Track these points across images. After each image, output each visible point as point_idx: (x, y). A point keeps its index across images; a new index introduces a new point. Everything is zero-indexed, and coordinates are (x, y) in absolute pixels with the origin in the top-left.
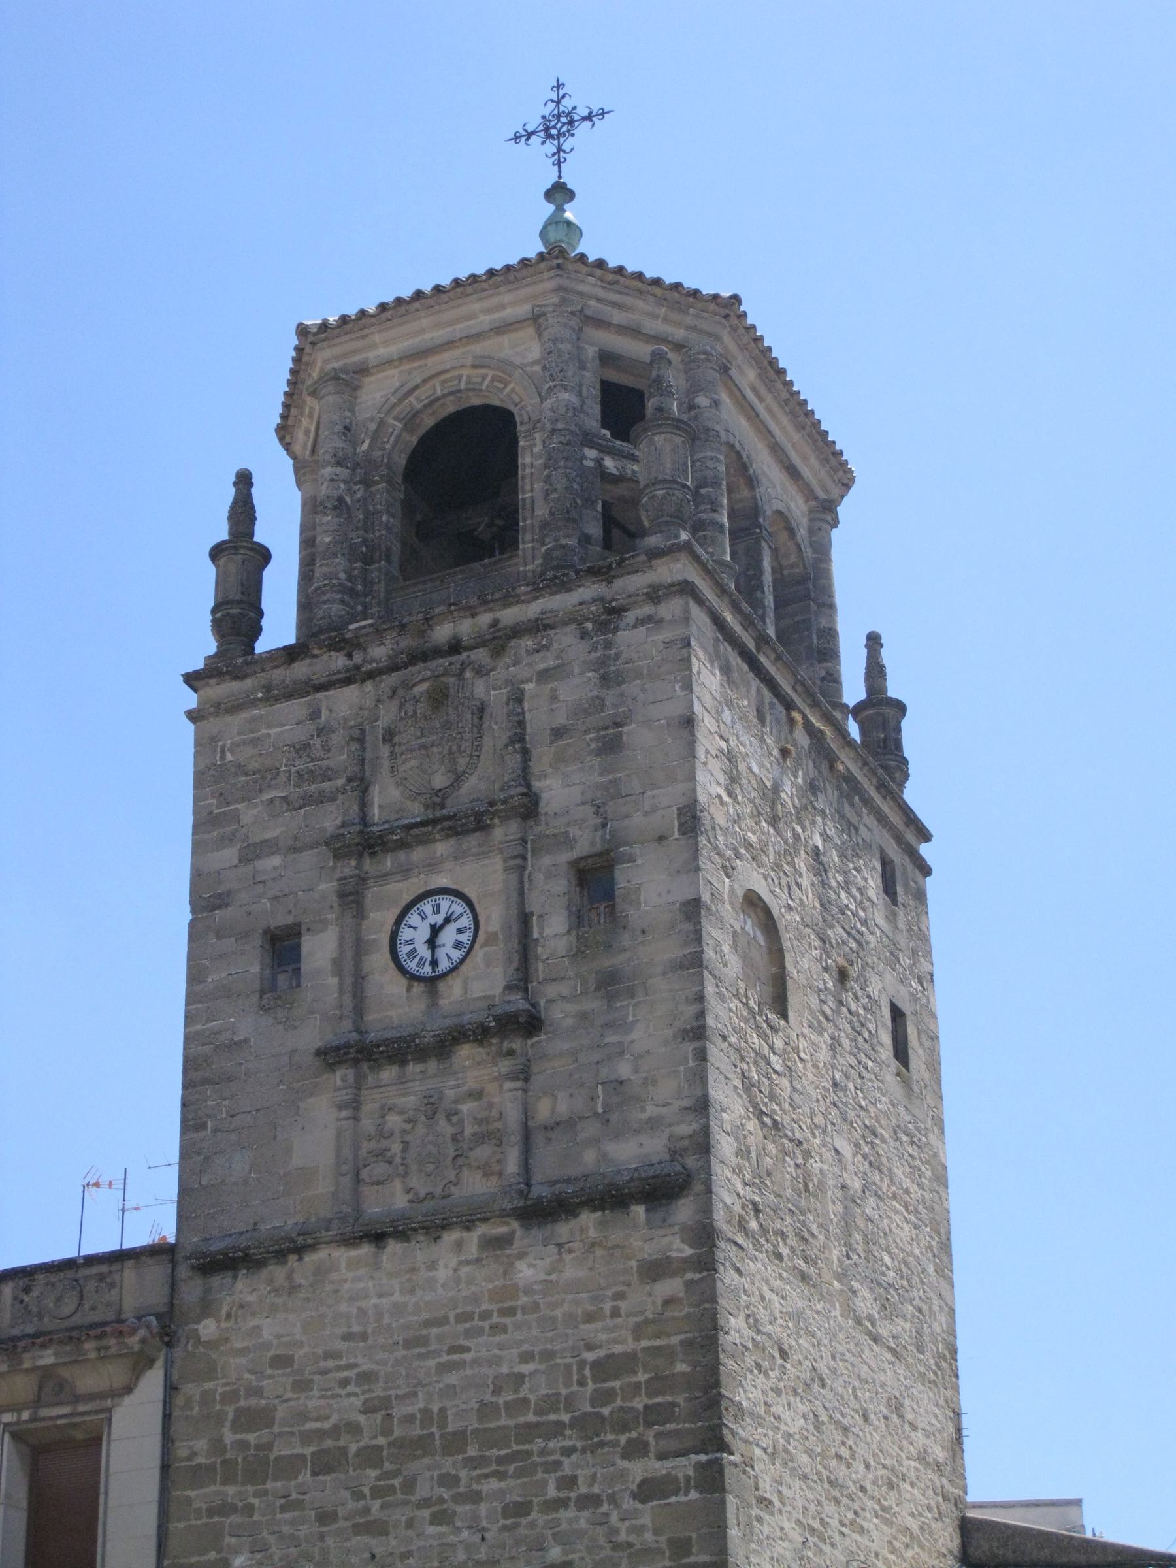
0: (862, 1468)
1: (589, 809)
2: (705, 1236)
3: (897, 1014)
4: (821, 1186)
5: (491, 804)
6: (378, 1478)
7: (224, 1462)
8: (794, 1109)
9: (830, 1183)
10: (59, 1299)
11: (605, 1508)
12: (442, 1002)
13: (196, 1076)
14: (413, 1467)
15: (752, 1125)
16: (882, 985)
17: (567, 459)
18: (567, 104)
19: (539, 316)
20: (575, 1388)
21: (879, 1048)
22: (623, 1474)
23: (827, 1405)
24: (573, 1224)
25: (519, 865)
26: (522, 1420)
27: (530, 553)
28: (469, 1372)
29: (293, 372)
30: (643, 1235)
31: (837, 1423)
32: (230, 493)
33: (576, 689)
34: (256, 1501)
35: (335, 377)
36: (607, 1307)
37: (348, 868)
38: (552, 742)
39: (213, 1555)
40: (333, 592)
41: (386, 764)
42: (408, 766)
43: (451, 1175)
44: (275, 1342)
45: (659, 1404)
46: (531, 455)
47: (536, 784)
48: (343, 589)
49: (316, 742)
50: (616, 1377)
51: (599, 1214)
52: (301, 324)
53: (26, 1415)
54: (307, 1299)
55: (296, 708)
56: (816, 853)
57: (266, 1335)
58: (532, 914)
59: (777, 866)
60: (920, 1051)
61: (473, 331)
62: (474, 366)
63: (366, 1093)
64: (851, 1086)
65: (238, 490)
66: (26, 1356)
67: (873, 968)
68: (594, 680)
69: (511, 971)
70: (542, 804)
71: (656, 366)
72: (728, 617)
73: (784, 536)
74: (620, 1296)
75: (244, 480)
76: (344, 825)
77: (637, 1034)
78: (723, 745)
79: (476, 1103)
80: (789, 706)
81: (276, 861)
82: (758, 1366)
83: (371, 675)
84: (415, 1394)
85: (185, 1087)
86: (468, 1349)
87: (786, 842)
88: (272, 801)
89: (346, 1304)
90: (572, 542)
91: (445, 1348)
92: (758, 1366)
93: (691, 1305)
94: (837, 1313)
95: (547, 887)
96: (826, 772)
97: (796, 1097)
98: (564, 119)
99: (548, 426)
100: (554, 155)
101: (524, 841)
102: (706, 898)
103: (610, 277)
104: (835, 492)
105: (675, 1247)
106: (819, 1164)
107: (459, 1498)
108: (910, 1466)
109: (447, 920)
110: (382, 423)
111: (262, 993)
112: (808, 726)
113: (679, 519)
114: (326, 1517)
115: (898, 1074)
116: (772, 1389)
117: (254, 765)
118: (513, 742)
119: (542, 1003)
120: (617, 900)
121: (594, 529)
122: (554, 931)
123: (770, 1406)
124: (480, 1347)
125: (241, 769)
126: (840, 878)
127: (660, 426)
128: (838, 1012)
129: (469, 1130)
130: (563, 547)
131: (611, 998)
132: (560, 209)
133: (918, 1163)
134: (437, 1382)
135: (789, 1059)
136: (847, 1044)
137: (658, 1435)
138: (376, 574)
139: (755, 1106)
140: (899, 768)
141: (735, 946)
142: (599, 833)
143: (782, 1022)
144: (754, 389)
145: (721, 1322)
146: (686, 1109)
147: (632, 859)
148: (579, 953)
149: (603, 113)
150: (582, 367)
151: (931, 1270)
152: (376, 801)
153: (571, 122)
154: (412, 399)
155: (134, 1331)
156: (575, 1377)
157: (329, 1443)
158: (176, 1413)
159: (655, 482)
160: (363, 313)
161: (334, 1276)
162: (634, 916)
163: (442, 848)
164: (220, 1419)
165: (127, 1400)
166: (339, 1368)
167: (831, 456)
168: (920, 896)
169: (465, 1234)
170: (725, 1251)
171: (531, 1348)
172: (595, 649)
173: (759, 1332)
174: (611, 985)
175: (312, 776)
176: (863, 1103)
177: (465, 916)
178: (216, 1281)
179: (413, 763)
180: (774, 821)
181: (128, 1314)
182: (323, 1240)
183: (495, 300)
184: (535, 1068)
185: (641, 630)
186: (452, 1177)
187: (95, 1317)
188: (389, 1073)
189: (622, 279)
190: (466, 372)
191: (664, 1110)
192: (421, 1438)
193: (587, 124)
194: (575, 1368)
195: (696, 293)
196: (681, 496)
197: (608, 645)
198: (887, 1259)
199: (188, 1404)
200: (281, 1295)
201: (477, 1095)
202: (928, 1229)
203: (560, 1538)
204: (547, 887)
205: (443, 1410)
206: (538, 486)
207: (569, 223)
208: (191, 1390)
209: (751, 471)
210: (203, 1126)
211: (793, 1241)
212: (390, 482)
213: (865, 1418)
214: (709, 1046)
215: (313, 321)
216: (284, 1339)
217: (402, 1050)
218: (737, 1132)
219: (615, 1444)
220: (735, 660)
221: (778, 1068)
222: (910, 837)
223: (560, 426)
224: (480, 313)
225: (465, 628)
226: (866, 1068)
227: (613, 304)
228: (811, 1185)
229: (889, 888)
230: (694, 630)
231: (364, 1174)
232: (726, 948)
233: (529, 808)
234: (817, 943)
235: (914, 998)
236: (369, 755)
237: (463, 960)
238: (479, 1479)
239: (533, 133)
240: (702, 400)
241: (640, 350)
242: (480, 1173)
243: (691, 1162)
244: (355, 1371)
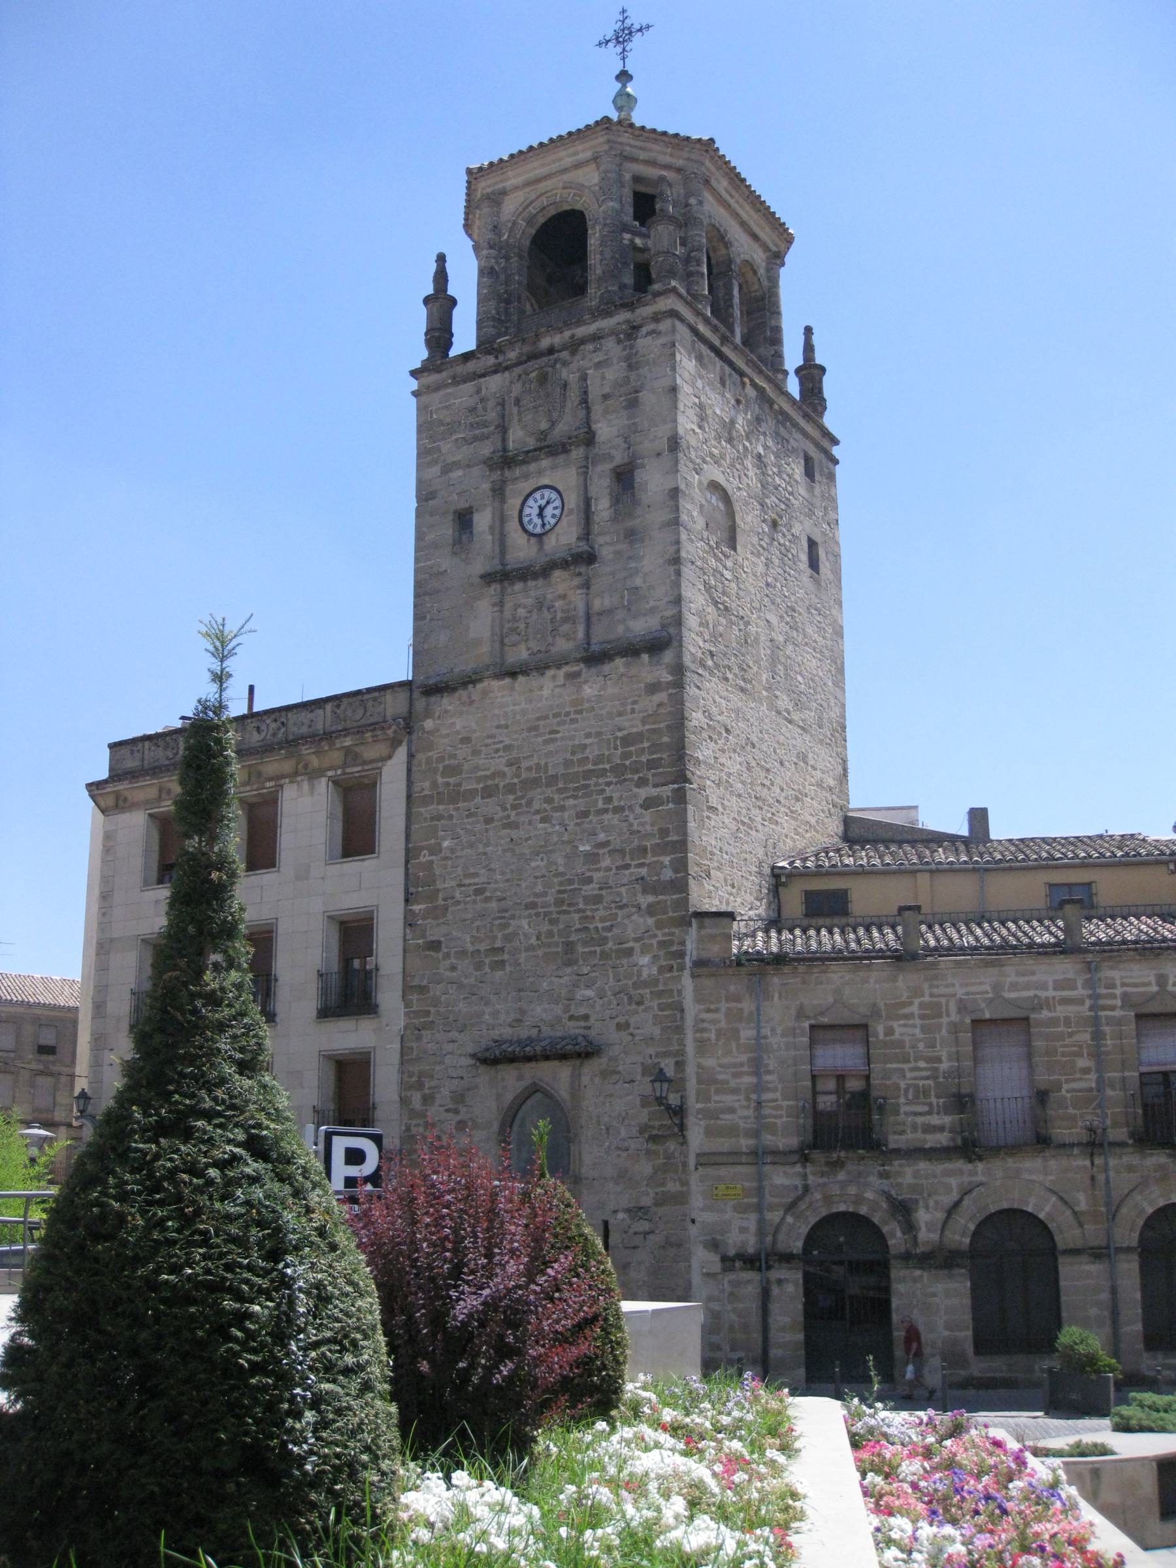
0: (778, 790)
1: (620, 440)
2: (679, 670)
3: (812, 544)
4: (757, 640)
5: (570, 438)
6: (515, 800)
7: (438, 793)
9: (763, 638)
10: (354, 711)
11: (627, 813)
12: (545, 547)
14: (531, 794)
15: (711, 609)
16: (801, 528)
18: (628, 22)
22: (635, 796)
24: (612, 665)
25: (585, 473)
26: (586, 768)
27: (594, 293)
29: (468, 195)
30: (649, 670)
31: (762, 767)
32: (433, 267)
33: (613, 373)
34: (454, 813)
35: (487, 197)
36: (629, 708)
37: (496, 475)
39: (433, 841)
41: (516, 418)
46: (593, 241)
47: (594, 426)
48: (494, 319)
49: (480, 406)
50: (633, 745)
53: (339, 772)
55: (469, 387)
56: (759, 456)
59: (732, 465)
64: (779, 585)
66: (337, 741)
72: (702, 328)
73: (750, 275)
74: (635, 702)
75: (441, 259)
76: (494, 452)
77: (645, 562)
78: (697, 400)
80: (742, 374)
81: (460, 473)
82: (710, 738)
83: (507, 368)
84: (532, 756)
85: (415, 597)
86: (558, 732)
87: (738, 451)
88: (457, 440)
90: (615, 288)
92: (710, 738)
94: (764, 708)
96: (767, 410)
97: (741, 593)
101: (587, 458)
102: (683, 487)
103: (637, 133)
104: (783, 246)
107: (555, 809)
108: (810, 789)
109: (548, 503)
110: (514, 223)
112: (754, 385)
113: (672, 274)
114: (489, 820)
117: (448, 420)
118: (581, 403)
119: (596, 546)
121: (628, 279)
122: (603, 507)
125: (441, 422)
126: (775, 470)
128: (771, 544)
131: (632, 543)
132: (624, 86)
133: (823, 625)
136: (776, 562)
137: (654, 775)
139: (713, 599)
140: (820, 404)
141: (701, 512)
144: (727, 192)
145: (687, 715)
147: (643, 466)
148: (614, 520)
149: (648, 27)
150: (623, 186)
151: (830, 684)
152: (511, 438)
153: (630, 33)
155: (389, 728)
157: (490, 782)
158: (414, 769)
159: (658, 253)
160: (501, 160)
161: (492, 695)
163: (545, 463)
164: (435, 771)
165: (389, 763)
166: (494, 743)
168: (831, 477)
170: (689, 677)
172: (625, 349)
173: (711, 720)
174: (632, 536)
175: (479, 425)
178: (433, 699)
179: (529, 417)
180: (730, 440)
181: (389, 718)
183: (572, 150)
184: (593, 581)
185: (649, 338)
187: (372, 720)
188: (518, 586)
190: (559, 191)
192: (535, 779)
193: (639, 34)
195: (688, 138)
197: (632, 347)
198: (800, 678)
199: (420, 765)
201: (563, 597)
203: (606, 829)
205: (546, 764)
206: (598, 257)
207: (629, 95)
208: (421, 757)
210: (425, 617)
211: (736, 670)
212: (521, 257)
213: (782, 764)
215: (475, 165)
217: (525, 574)
218: (700, 614)
219: (631, 780)
220: (705, 350)
221: (729, 577)
222: (825, 443)
223: (608, 221)
224: (566, 157)
225: (557, 339)
227: (641, 148)
229: (809, 473)
230: (678, 337)
231: (506, 641)
232: (695, 514)
233: (589, 439)
234: (759, 507)
235: (824, 534)
236: (507, 413)
238: (564, 799)
240: (693, 201)
241: (652, 172)
243: (672, 630)
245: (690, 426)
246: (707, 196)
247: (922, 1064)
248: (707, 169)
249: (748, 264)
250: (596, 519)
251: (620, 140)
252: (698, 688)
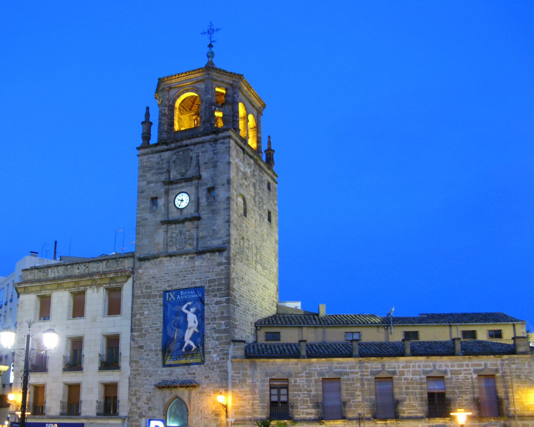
2: (228, 258)
12: (183, 213)
13: (138, 224)
32: (145, 111)
36: (211, 270)
75: (148, 108)
81: (153, 185)
129: (187, 237)
170: (232, 261)
178: (142, 262)
184: (200, 226)
218: (235, 239)
240: (235, 96)
243: (227, 245)
247: (305, 392)
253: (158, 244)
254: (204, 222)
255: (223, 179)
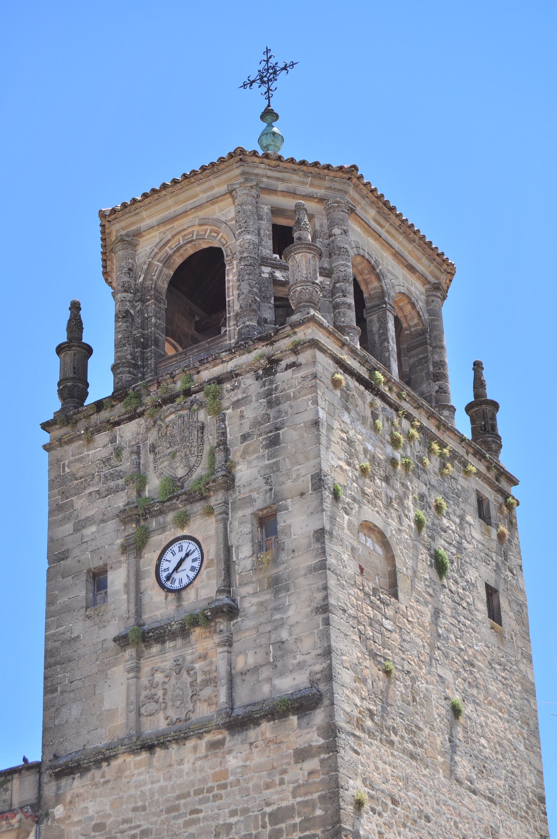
2: (331, 731)
3: (491, 592)
8: (403, 652)
12: (185, 603)
13: (52, 660)
17: (249, 274)
18: (272, 62)
19: (232, 191)
20: (260, 829)
21: (476, 613)
23: (432, 833)
24: (259, 730)
27: (232, 330)
28: (201, 825)
30: (302, 733)
32: (67, 315)
36: (277, 779)
38: (242, 443)
40: (123, 367)
42: (163, 465)
43: (190, 706)
44: (96, 816)
45: (307, 836)
46: (231, 278)
48: (129, 365)
50: (283, 822)
51: (272, 722)
52: (101, 211)
54: (113, 788)
57: (91, 812)
58: (232, 546)
60: (511, 614)
61: (197, 204)
62: (200, 225)
63: (144, 661)
64: (452, 636)
65: (72, 312)
67: (471, 564)
68: (264, 404)
69: (220, 582)
70: (236, 480)
71: (297, 213)
74: (284, 772)
75: (75, 307)
76: (128, 504)
77: (291, 612)
78: (344, 436)
79: (203, 662)
81: (93, 529)
85: (46, 668)
86: (201, 811)
88: (90, 494)
89: (134, 790)
90: (254, 323)
91: (188, 811)
93: (323, 774)
95: (240, 530)
97: (404, 644)
98: (271, 71)
99: (238, 255)
100: (265, 93)
101: (226, 503)
104: (443, 278)
105: (314, 739)
106: (425, 685)
109: (187, 555)
110: (150, 264)
111: (87, 608)
115: (492, 628)
116: (385, 824)
117: (81, 473)
118: (218, 445)
119: (238, 598)
120: (279, 533)
121: (269, 314)
122: (244, 554)
123: (383, 834)
124: (207, 809)
127: (298, 248)
129: (200, 678)
130: (247, 326)
131: (277, 592)
132: (270, 125)
134: (185, 832)
135: (400, 622)
136: (448, 611)
138: (149, 354)
142: (268, 494)
143: (393, 600)
146: (319, 655)
148: (256, 569)
149: (293, 64)
150: (260, 218)
151: (522, 748)
153: (275, 73)
154: (167, 248)
156: (260, 823)
161: (128, 773)
162: (289, 543)
167: (436, 257)
169: (199, 741)
170: (343, 739)
171: (235, 808)
172: (264, 385)
174: (277, 585)
176: (463, 647)
177: (196, 551)
178: (64, 782)
179: (166, 463)
181: (16, 805)
182: (120, 752)
184: (235, 638)
185: (290, 371)
186: (191, 708)
188: (155, 649)
189: (281, 164)
190: (196, 229)
191: (307, 657)
194: (260, 817)
196: (311, 289)
198: (483, 741)
200: (98, 788)
201: (204, 657)
202: (519, 722)
204: (240, 530)
206: (236, 292)
207: (274, 133)
209: (378, 270)
210: (56, 690)
214: (332, 616)
215: (107, 209)
216: (101, 814)
218: (355, 667)
221: (389, 627)
222: (504, 484)
223: (245, 255)
224: (200, 192)
226: (465, 625)
227: (278, 179)
228: (418, 698)
231: (143, 710)
232: (345, 557)
236: (142, 462)
237: (195, 578)
239: (254, 81)
240: (337, 231)
241: (289, 203)
242: (206, 704)
243: (322, 687)
244: (139, 829)
245: (336, 462)
246: (353, 225)
248: (353, 198)
249: (407, 296)
250: (238, 568)
251: (256, 171)
252: (356, 752)
253: (112, 713)
254: (249, 623)
255: (298, 477)
